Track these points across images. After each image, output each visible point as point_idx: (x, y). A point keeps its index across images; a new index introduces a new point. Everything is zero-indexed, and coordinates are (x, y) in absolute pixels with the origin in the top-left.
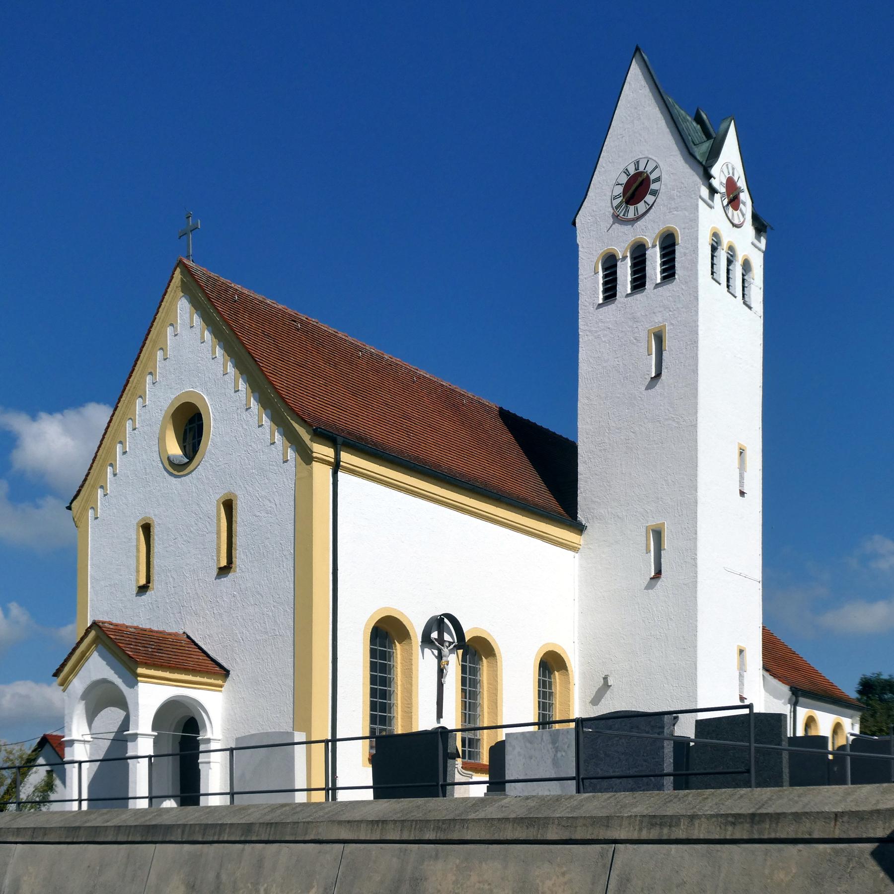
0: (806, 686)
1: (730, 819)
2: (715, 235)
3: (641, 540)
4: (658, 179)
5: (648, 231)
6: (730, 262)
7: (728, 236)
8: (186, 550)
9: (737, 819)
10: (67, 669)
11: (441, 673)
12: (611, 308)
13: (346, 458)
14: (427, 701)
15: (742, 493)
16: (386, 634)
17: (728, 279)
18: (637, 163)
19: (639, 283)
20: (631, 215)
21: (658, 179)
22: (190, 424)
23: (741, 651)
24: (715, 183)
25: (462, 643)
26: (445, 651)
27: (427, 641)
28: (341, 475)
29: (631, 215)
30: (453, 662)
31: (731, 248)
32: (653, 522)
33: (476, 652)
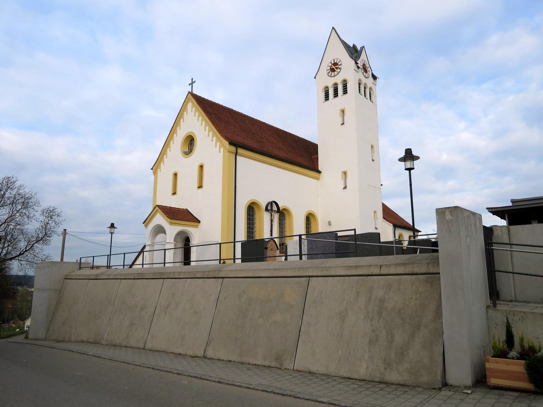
0: (399, 224)
1: (347, 268)
2: (360, 80)
3: (340, 175)
4: (341, 65)
5: (339, 79)
6: (365, 88)
7: (364, 80)
8: (188, 179)
9: (350, 267)
10: (147, 221)
11: (272, 221)
12: (328, 102)
13: (240, 151)
14: (266, 228)
15: (373, 160)
16: (251, 209)
17: (365, 94)
18: (334, 60)
19: (336, 95)
20: (333, 75)
21: (341, 65)
22: (190, 141)
23: (375, 212)
24: (359, 65)
25: (279, 211)
26: (273, 213)
27: (267, 209)
28: (237, 156)
29: (333, 75)
30: (276, 216)
31: (365, 84)
32: (344, 170)
33: (283, 214)
